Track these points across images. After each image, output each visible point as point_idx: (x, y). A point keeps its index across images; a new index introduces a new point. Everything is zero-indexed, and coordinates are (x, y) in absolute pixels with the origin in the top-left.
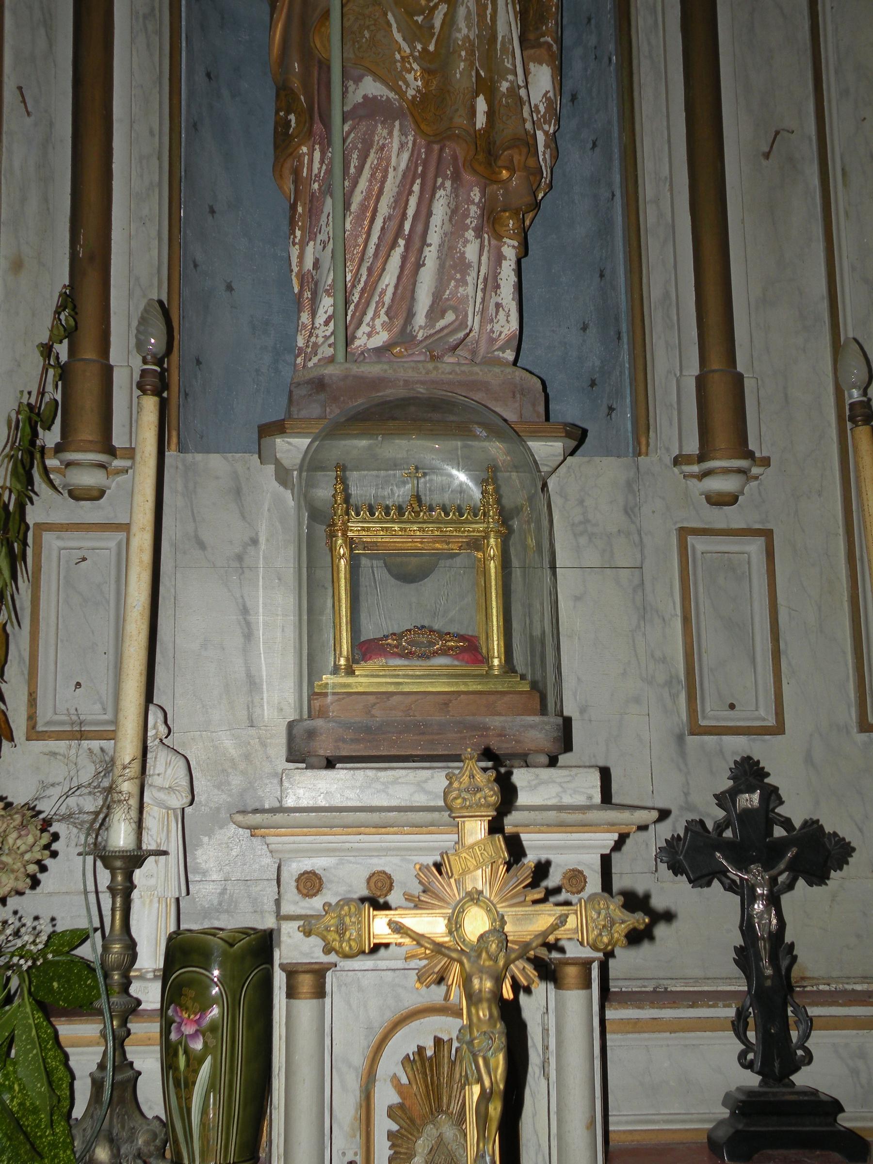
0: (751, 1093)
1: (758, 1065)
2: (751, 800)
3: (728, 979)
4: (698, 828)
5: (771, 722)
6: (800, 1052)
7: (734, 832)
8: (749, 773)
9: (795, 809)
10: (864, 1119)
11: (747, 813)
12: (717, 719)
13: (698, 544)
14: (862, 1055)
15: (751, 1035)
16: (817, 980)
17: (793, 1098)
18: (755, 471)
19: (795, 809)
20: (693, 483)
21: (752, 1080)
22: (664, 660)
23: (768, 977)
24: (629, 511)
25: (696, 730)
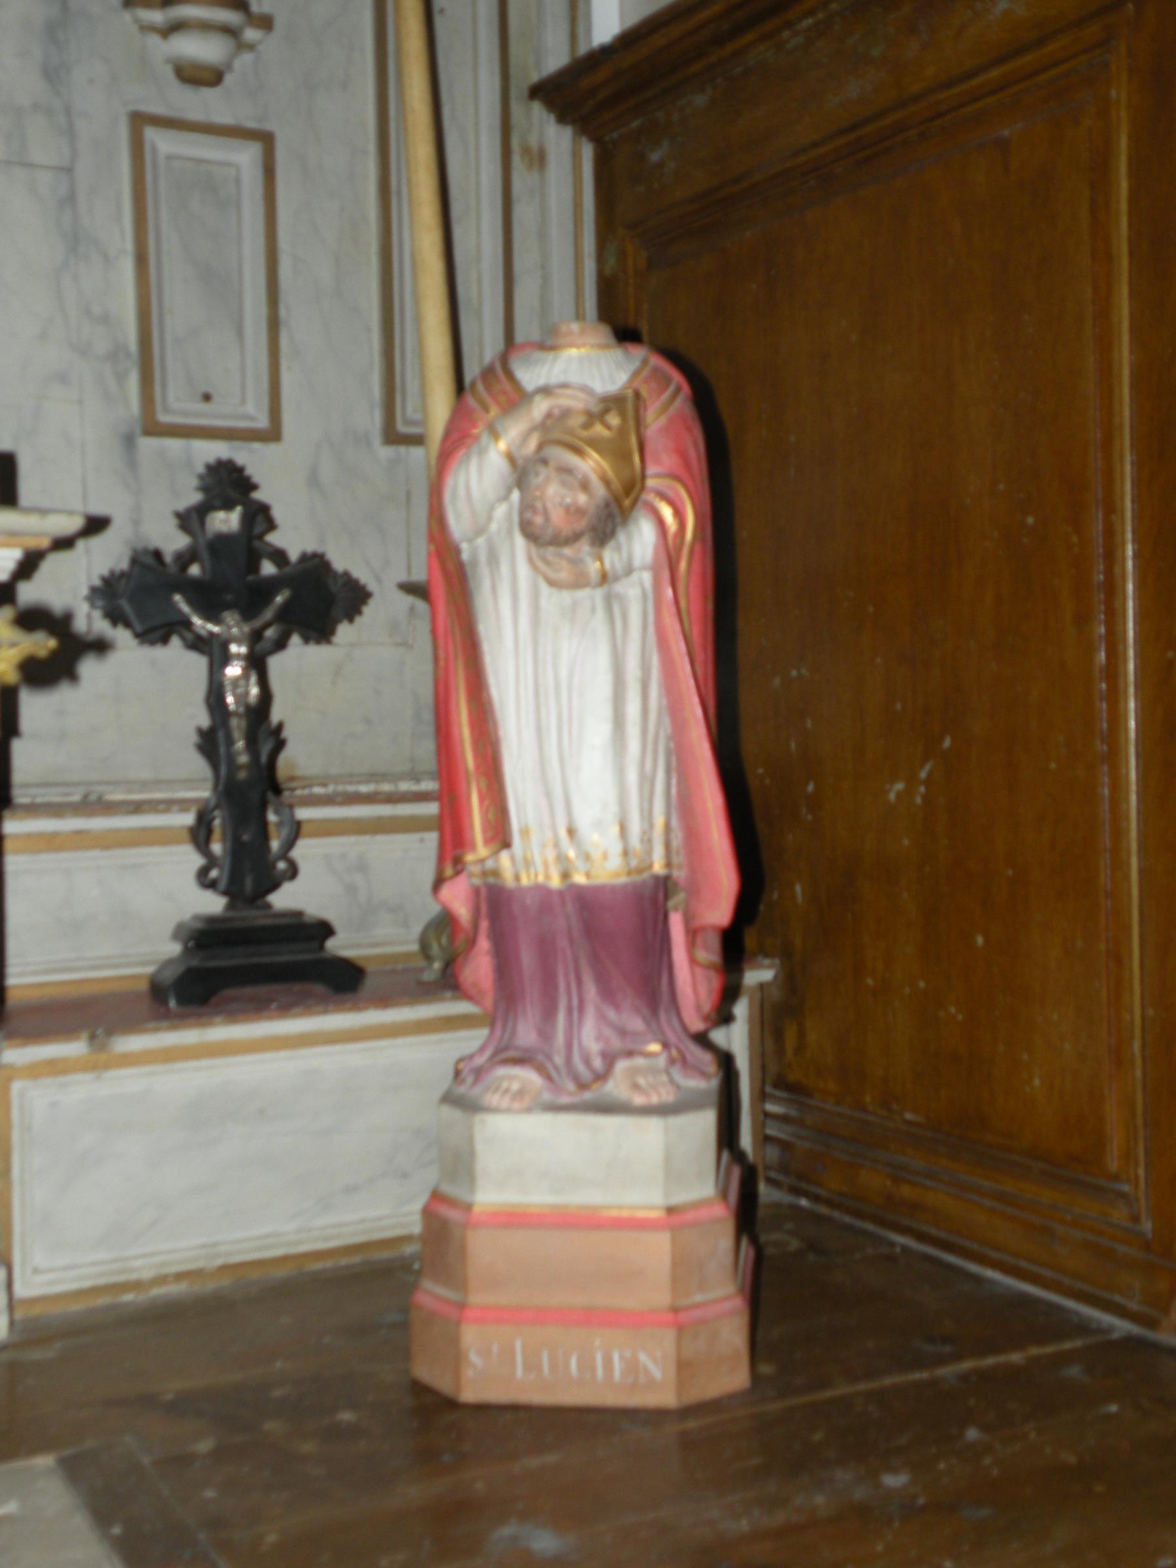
0: (211, 920)
1: (222, 885)
2: (227, 521)
3: (189, 783)
4: (150, 560)
5: (262, 422)
6: (281, 865)
7: (203, 568)
8: (228, 483)
9: (292, 537)
10: (358, 946)
11: (221, 543)
12: (185, 414)
13: (161, 142)
14: (362, 866)
15: (217, 848)
16: (309, 782)
17: (268, 922)
18: (251, 34)
19: (292, 537)
20: (154, 40)
21: (214, 904)
22: (105, 320)
23: (241, 767)
24: (53, 74)
25: (153, 428)
